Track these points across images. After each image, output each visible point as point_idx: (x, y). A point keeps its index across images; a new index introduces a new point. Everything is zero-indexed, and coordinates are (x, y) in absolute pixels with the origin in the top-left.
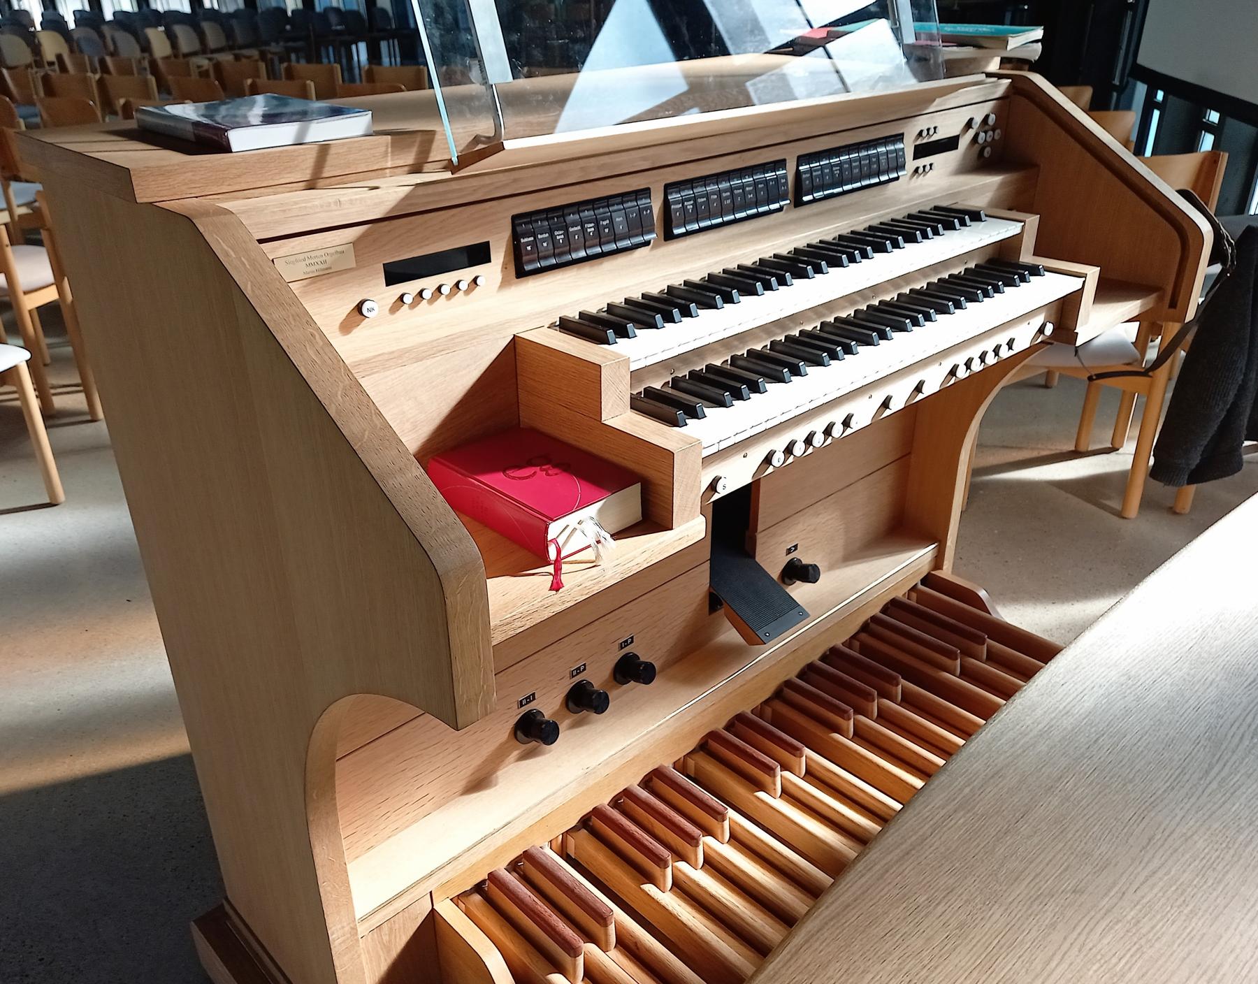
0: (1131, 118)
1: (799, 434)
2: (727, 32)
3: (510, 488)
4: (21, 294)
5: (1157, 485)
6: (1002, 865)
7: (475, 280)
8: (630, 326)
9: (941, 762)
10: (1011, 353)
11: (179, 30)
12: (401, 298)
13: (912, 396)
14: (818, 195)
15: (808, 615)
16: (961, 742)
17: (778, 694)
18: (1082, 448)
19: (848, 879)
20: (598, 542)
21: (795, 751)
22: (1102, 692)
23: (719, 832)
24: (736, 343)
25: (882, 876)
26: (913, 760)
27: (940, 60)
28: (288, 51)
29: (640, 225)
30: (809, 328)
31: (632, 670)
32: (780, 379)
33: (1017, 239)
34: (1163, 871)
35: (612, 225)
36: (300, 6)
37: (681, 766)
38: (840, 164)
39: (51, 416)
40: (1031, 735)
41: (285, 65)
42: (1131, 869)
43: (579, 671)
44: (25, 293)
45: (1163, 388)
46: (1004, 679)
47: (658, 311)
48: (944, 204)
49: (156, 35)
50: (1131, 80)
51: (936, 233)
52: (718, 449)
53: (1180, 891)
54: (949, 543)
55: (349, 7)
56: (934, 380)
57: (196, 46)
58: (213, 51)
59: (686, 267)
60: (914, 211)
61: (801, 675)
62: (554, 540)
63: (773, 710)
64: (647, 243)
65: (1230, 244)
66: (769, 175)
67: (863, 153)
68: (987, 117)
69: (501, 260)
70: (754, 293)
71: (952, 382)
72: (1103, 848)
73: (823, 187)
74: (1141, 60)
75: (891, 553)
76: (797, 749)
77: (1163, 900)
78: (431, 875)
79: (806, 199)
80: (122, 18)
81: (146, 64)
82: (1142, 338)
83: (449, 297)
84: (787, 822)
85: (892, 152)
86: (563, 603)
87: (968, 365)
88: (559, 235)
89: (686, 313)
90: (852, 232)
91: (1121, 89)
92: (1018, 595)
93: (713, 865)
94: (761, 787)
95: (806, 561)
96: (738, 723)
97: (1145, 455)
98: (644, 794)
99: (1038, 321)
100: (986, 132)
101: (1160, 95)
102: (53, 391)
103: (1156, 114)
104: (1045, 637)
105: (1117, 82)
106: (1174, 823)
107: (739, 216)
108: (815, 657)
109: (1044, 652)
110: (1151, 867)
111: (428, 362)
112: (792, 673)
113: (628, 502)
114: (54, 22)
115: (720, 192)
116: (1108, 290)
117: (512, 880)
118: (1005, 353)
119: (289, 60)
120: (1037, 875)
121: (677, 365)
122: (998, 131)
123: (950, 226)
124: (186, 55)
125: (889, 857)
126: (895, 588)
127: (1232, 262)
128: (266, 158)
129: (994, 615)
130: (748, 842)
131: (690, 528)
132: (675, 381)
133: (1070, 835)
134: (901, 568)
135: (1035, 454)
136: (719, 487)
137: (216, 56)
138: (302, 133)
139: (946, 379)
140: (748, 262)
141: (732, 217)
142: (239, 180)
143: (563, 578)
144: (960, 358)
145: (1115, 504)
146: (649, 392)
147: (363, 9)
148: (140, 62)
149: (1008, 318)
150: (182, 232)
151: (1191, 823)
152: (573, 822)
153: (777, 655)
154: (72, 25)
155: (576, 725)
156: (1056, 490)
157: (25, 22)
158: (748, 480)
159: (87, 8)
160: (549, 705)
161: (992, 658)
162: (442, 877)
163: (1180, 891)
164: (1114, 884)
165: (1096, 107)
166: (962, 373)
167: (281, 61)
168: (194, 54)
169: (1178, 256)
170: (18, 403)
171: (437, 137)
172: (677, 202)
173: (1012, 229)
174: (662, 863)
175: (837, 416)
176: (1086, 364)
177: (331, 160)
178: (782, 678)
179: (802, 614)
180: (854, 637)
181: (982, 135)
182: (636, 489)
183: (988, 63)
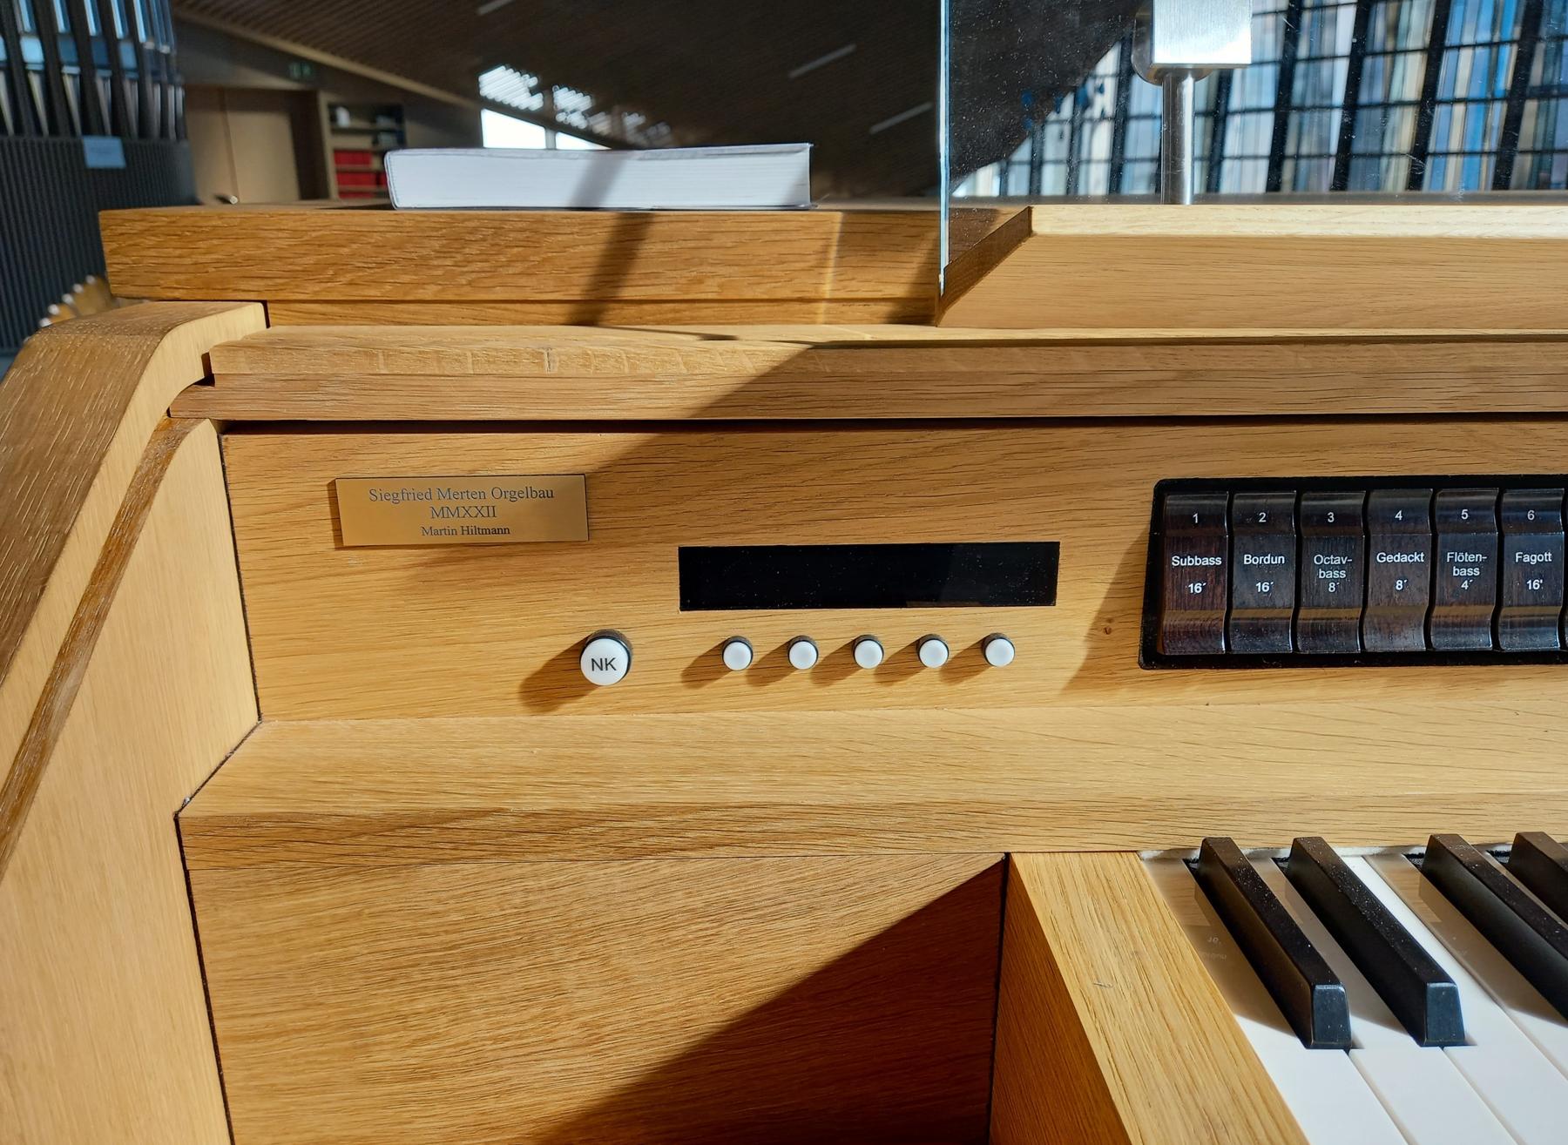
69: (1095, 604)
101: (1535, 584)
111: (666, 868)
138: (599, 180)
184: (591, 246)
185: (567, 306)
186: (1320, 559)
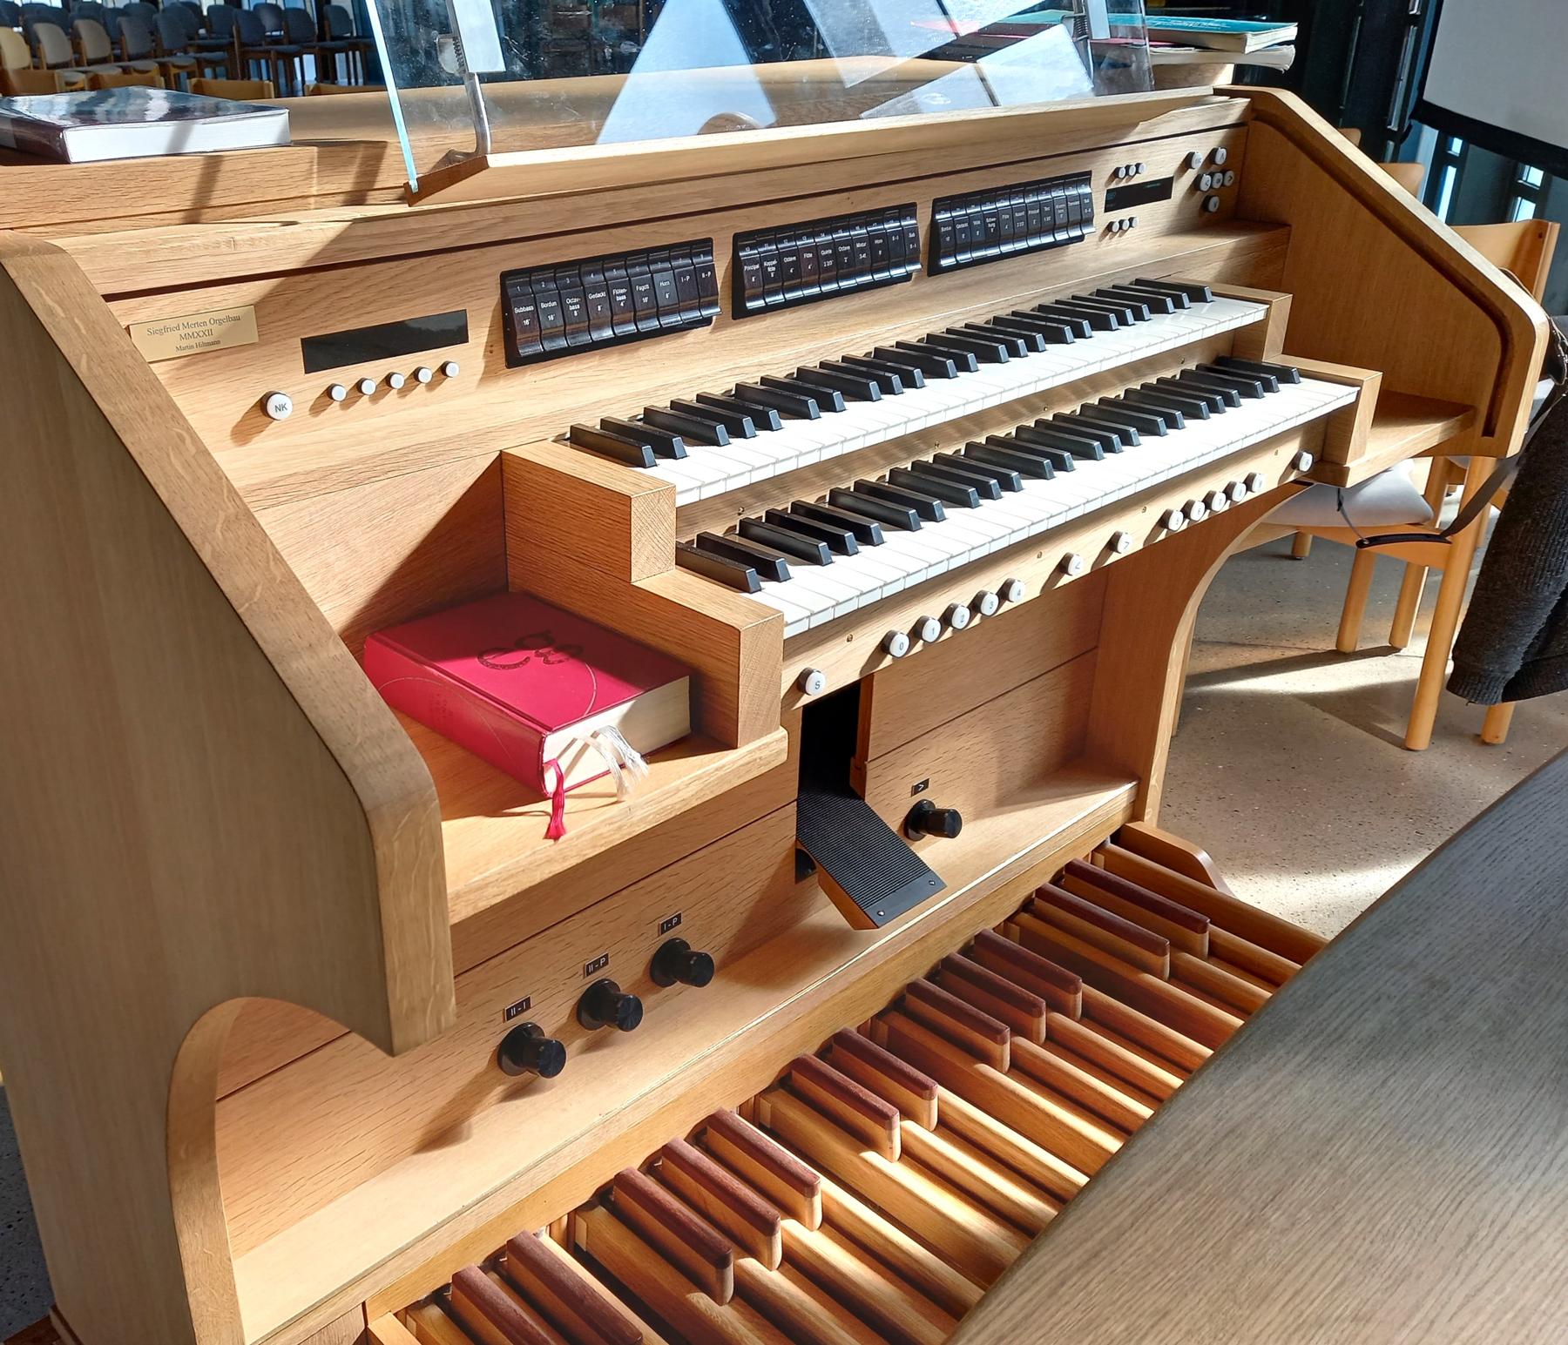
0: (1420, 171)
2: (833, 40)
3: (487, 682)
6: (1242, 1276)
7: (443, 369)
8: (677, 440)
10: (1250, 496)
11: (42, 30)
12: (328, 392)
15: (942, 886)
17: (898, 1004)
18: (1347, 647)
19: (1002, 1296)
21: (923, 1090)
24: (838, 471)
27: (1146, 66)
28: (201, 64)
29: (698, 291)
30: (949, 451)
31: (678, 965)
33: (1258, 329)
37: (751, 1111)
41: (194, 80)
42: (1443, 1284)
43: (597, 965)
45: (1466, 563)
46: (1234, 985)
50: (1414, 122)
51: (1139, 317)
52: (809, 619)
53: (1520, 1320)
54: (1153, 782)
55: (290, 5)
56: (1134, 532)
57: (67, 54)
59: (764, 358)
60: (1106, 286)
61: (932, 976)
62: (554, 762)
63: (892, 1030)
64: (706, 321)
67: (1031, 199)
68: (1213, 153)
70: (867, 397)
71: (1162, 536)
72: (1398, 1250)
74: (1428, 96)
75: (1066, 796)
77: (1494, 1334)
78: (363, 1276)
79: (945, 262)
82: (1435, 487)
83: (403, 392)
84: (909, 1198)
85: (1073, 198)
86: (565, 859)
87: (1186, 511)
88: (574, 305)
89: (764, 424)
90: (1014, 313)
91: (1400, 137)
93: (799, 1264)
94: (869, 1143)
95: (940, 804)
96: (837, 1047)
97: (1439, 661)
98: (693, 1153)
99: (1290, 449)
100: (1212, 175)
101: (1457, 145)
103: (1451, 172)
105: (1394, 127)
107: (844, 284)
108: (952, 949)
110: (1475, 1280)
112: (918, 972)
113: (668, 706)
115: (815, 249)
116: (1393, 409)
117: (489, 1284)
118: (1241, 496)
119: (202, 75)
120: (1297, 1293)
121: (749, 501)
122: (1230, 173)
125: (1067, 1261)
126: (1074, 847)
128: (121, 175)
131: (765, 747)
132: (745, 528)
133: (1346, 1230)
134: (1081, 817)
135: (1277, 655)
136: (810, 686)
138: (180, 138)
140: (859, 352)
142: (79, 205)
143: (566, 820)
144: (1175, 502)
145: (1395, 729)
146: (705, 541)
151: (1534, 1213)
152: (585, 1196)
153: (896, 946)
155: (593, 1046)
158: (850, 675)
160: (551, 1017)
161: (1217, 952)
162: (385, 1279)
163: (1520, 1320)
164: (1417, 1307)
165: (1374, 150)
166: (1177, 524)
167: (190, 76)
168: (65, 65)
169: (1497, 357)
171: (389, 151)
172: (752, 261)
173: (1248, 314)
176: (1354, 522)
177: (222, 182)
180: (1010, 919)
181: (1206, 178)
182: (683, 684)
183: (1215, 74)
184: (191, 177)
185: (1221, 133)
186: (569, 301)
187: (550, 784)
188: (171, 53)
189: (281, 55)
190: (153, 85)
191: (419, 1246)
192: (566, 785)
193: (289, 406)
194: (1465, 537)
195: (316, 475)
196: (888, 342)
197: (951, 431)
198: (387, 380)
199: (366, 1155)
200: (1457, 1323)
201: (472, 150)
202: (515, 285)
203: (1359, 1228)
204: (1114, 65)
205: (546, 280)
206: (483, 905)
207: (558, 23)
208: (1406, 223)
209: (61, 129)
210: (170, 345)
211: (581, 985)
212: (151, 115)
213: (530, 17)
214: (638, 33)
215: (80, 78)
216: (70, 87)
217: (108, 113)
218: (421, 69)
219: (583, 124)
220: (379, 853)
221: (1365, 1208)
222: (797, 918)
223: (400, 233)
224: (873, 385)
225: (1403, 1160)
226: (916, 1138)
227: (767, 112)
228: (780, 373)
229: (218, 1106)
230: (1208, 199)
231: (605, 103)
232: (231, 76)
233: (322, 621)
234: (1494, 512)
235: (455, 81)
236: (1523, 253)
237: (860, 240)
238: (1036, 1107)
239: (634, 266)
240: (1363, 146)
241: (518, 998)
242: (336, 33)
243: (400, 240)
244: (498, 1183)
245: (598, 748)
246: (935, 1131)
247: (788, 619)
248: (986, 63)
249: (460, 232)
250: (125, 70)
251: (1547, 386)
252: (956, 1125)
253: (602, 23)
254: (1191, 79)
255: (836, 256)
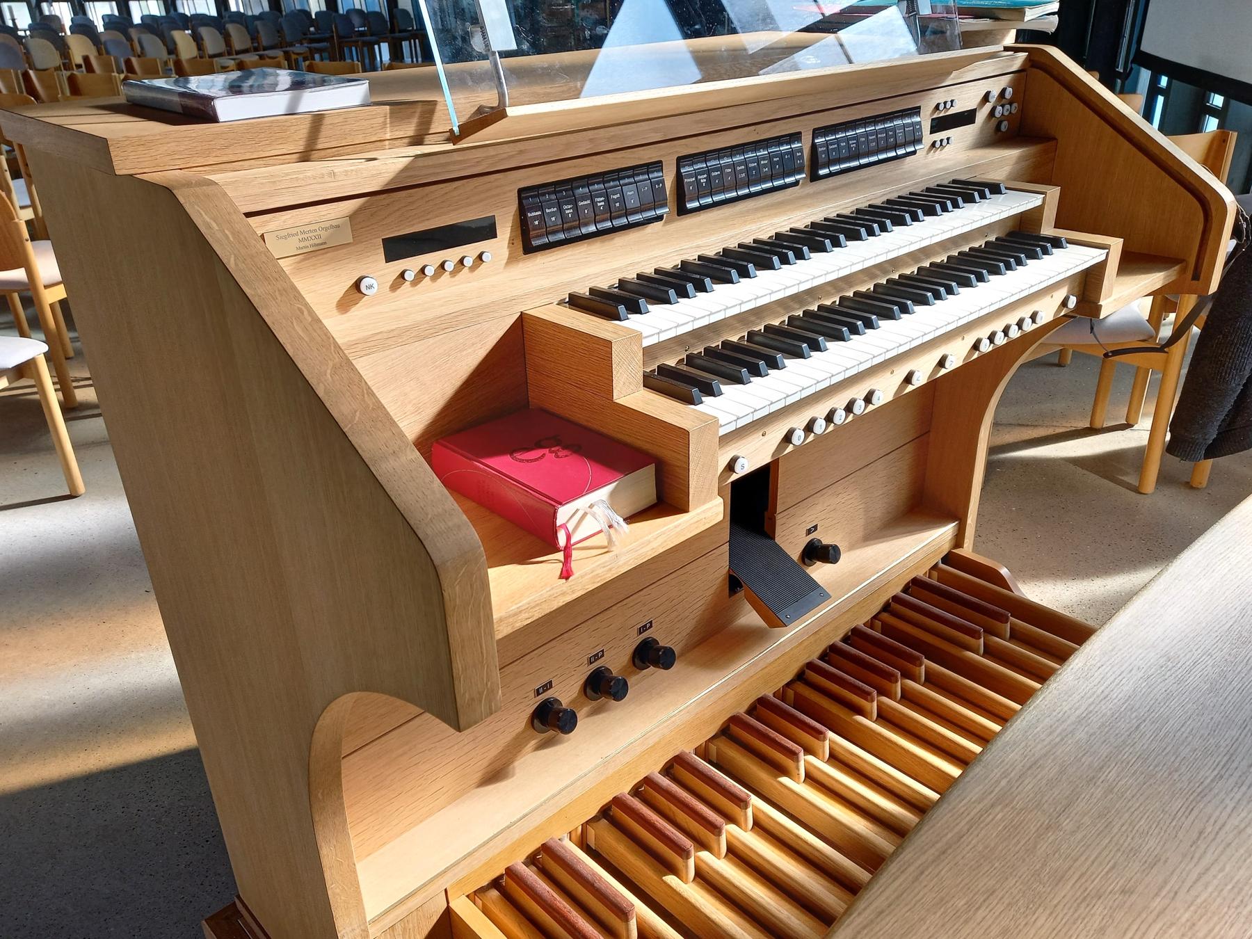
0: (1140, 99)
1: (820, 411)
2: (739, 21)
3: (518, 471)
4: (41, 288)
5: (1174, 460)
6: (1044, 865)
7: (480, 257)
8: (642, 301)
9: (977, 749)
10: (1035, 326)
11: (204, 31)
12: (402, 275)
13: (935, 371)
14: (834, 168)
16: (996, 728)
17: (800, 677)
18: (1098, 425)
20: (610, 527)
21: (818, 734)
22: (1140, 675)
23: (742, 820)
24: (753, 318)
25: (916, 879)
26: (927, 736)
28: (312, 52)
30: (828, 302)
31: (650, 655)
32: (800, 355)
33: (1039, 211)
34: (1217, 867)
35: (623, 199)
36: (324, 8)
37: (703, 752)
38: (856, 138)
39: (71, 409)
40: (1069, 722)
41: (307, 63)
42: (1183, 866)
43: (596, 657)
44: (46, 287)
45: (1180, 360)
46: (1029, 658)
47: (671, 285)
48: (963, 177)
49: (182, 38)
51: (956, 205)
52: (736, 424)
53: (1236, 890)
57: (222, 47)
58: (238, 53)
60: (932, 185)
61: (823, 657)
62: (564, 526)
63: (796, 694)
64: (660, 218)
65: (1245, 220)
66: (784, 148)
68: (1004, 90)
70: (771, 267)
71: (976, 355)
72: (1151, 843)
73: (839, 161)
74: (1146, 47)
75: (911, 532)
76: (820, 733)
77: (1219, 900)
79: (822, 172)
80: (150, 23)
81: (171, 65)
86: (573, 592)
87: (991, 338)
88: (568, 210)
89: (701, 288)
90: (870, 206)
91: (1125, 76)
92: (1038, 572)
93: (736, 854)
94: (784, 771)
95: (825, 541)
96: (760, 707)
98: (665, 782)
99: (1061, 294)
100: (1003, 106)
101: (1164, 81)
102: (75, 384)
103: (1161, 99)
104: (1066, 613)
106: (1225, 815)
107: (753, 189)
108: (836, 639)
109: (1079, 633)
111: (431, 341)
113: (643, 484)
114: (83, 27)
115: (734, 165)
116: (1132, 262)
117: (530, 874)
118: (1029, 327)
119: (313, 59)
121: (692, 341)
122: (1015, 105)
123: (969, 199)
124: (211, 57)
125: (923, 858)
127: (1247, 236)
128: (256, 129)
129: (1016, 593)
130: (772, 829)
131: (708, 510)
132: (690, 360)
134: (922, 547)
135: (1050, 431)
136: (738, 467)
137: (241, 56)
138: (294, 102)
139: (970, 353)
140: (764, 236)
141: (747, 191)
142: (227, 151)
143: (574, 565)
144: (983, 333)
145: (1131, 479)
146: (663, 370)
147: (385, 13)
148: (166, 63)
149: (1031, 290)
150: (161, 202)
151: (1243, 815)
152: (593, 812)
153: (798, 639)
154: (101, 29)
155: (595, 712)
156: (1072, 467)
157: (54, 26)
159: (116, 13)
160: (566, 693)
161: (1016, 636)
162: (461, 871)
163: (1236, 890)
164: (1166, 882)
166: (986, 347)
169: (1201, 227)
170: (37, 397)
171: (439, 107)
173: (1033, 201)
174: (684, 853)
175: (858, 392)
177: (325, 131)
178: (804, 660)
179: (824, 596)
180: (875, 617)
181: (999, 108)
182: (648, 473)
183: (1004, 36)
187: (562, 541)
188: (291, 45)
189: (365, 44)
190: (279, 66)
191: (482, 850)
192: (573, 541)
193: (375, 285)
194: (1177, 349)
195: (395, 333)
196: (784, 228)
197: (829, 288)
198: (442, 266)
199: (445, 790)
200: (1193, 893)
201: (495, 104)
202: (527, 198)
203: (1124, 828)
204: (935, 32)
205: (549, 193)
206: (519, 625)
207: (552, 15)
208: (1136, 135)
209: (212, 99)
210: (292, 246)
211: (587, 671)
212: (281, 86)
213: (532, 10)
214: (607, 20)
215: (231, 63)
216: (224, 69)
217: (251, 86)
218: (459, 51)
219: (572, 84)
220: (445, 594)
221: (1127, 815)
222: (731, 621)
223: (448, 164)
224: (775, 259)
225: (1152, 781)
226: (816, 767)
227: (696, 73)
228: (711, 252)
229: (344, 762)
230: (1000, 123)
231: (584, 70)
232: (332, 59)
233: (401, 435)
234: (1195, 330)
235: (485, 58)
236: (1212, 154)
237: (764, 159)
238: (895, 744)
239: (609, 181)
240: (1102, 81)
241: (545, 681)
242: (403, 27)
243: (452, 168)
244: (533, 806)
245: (594, 515)
246: (828, 762)
247: (722, 422)
248: (843, 34)
249: (490, 161)
250: (261, 57)
251: (1234, 242)
252: (841, 757)
253: (583, 13)
254: (987, 41)
255: (748, 170)
